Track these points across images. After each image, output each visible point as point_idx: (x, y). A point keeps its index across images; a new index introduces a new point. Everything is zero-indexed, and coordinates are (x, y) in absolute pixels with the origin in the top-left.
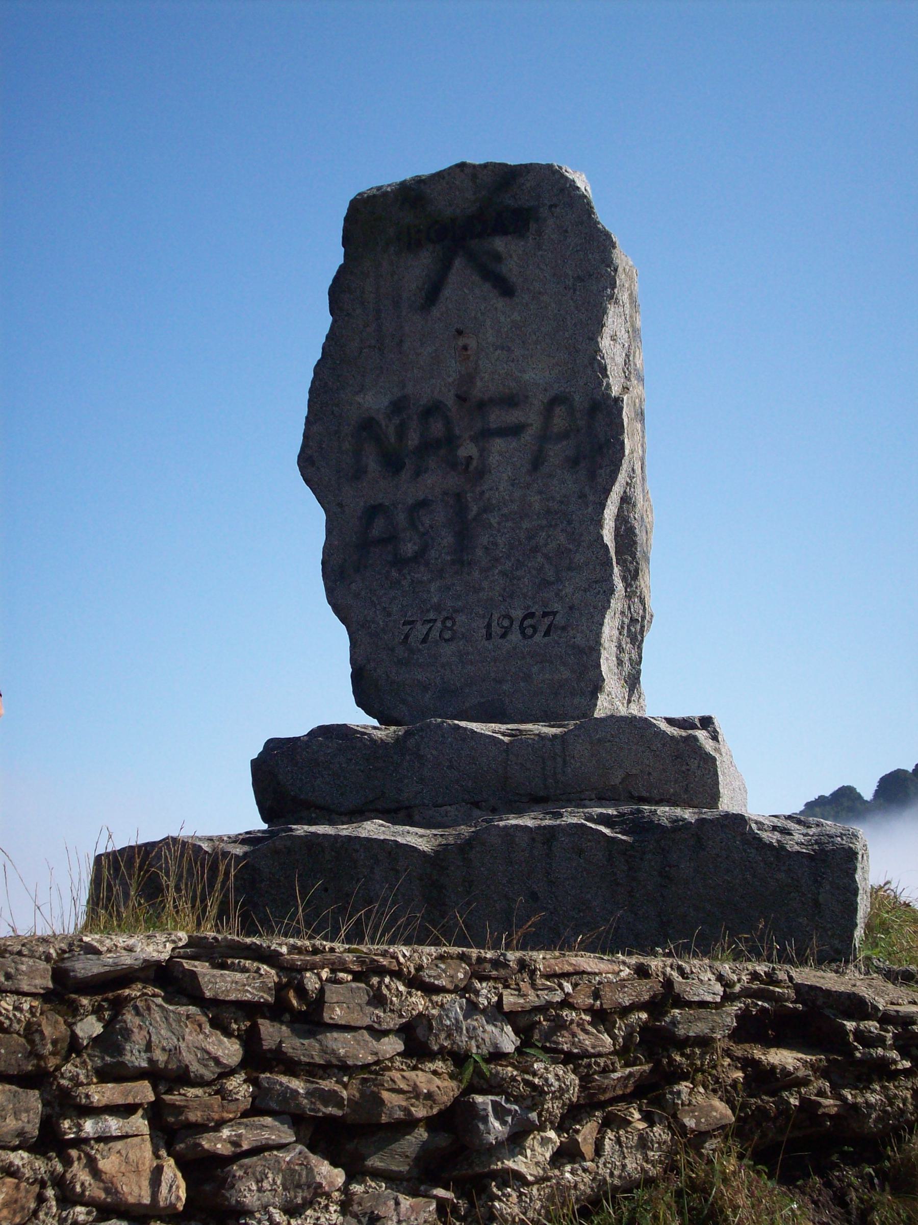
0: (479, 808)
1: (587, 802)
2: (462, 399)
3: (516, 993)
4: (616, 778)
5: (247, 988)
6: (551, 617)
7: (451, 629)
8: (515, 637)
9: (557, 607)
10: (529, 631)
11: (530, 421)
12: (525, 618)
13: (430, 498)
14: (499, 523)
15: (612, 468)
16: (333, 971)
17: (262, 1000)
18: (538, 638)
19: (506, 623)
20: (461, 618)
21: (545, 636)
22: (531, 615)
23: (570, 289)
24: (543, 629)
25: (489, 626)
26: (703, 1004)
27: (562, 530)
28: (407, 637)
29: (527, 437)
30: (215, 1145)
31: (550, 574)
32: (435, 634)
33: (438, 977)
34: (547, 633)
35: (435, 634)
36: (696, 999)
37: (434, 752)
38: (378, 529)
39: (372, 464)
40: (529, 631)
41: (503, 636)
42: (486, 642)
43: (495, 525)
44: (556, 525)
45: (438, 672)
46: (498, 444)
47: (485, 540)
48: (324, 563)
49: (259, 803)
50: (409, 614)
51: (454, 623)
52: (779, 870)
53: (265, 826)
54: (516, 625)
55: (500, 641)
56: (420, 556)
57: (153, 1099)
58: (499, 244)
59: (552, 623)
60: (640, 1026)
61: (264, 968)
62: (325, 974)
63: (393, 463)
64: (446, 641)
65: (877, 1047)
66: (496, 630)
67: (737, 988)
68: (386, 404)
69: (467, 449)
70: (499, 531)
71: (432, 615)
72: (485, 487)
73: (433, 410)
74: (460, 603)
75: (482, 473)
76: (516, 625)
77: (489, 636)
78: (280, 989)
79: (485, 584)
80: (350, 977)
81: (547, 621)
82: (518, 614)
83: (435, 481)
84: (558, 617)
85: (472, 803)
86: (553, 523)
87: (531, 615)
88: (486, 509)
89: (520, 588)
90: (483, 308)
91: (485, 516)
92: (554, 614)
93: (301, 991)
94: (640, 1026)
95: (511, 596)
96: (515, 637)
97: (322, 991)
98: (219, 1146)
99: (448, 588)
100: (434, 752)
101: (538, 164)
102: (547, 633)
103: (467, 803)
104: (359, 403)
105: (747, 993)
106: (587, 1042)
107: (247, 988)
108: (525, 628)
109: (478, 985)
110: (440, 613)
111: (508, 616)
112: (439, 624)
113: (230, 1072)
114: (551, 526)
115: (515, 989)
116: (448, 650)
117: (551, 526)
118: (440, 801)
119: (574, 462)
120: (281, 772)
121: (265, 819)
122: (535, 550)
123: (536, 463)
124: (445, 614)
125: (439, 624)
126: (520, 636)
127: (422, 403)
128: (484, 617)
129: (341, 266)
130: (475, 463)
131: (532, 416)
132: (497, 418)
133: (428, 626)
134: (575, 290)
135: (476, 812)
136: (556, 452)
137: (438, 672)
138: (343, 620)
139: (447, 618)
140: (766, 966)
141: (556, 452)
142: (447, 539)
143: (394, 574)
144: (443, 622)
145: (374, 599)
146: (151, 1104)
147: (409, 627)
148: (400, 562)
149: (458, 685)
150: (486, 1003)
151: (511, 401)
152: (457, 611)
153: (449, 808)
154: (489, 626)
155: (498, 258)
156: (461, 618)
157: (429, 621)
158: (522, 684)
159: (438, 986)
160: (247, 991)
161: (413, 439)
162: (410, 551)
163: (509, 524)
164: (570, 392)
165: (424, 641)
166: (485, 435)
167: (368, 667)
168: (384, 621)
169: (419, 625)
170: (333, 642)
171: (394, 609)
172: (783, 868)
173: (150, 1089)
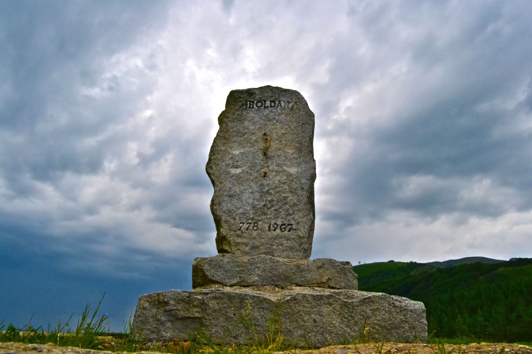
4: (324, 280)
7: (256, 226)
9: (293, 222)
10: (283, 230)
18: (286, 232)
20: (260, 223)
22: (284, 224)
24: (288, 229)
25: (269, 227)
31: (291, 211)
32: (251, 227)
34: (289, 231)
35: (251, 227)
40: (283, 230)
41: (274, 230)
64: (255, 230)
71: (250, 221)
76: (279, 227)
77: (269, 230)
79: (269, 212)
81: (289, 227)
82: (279, 223)
84: (293, 226)
87: (284, 224)
92: (292, 225)
99: (256, 213)
102: (289, 231)
111: (276, 224)
112: (252, 225)
116: (255, 233)
118: (264, 283)
122: (286, 203)
125: (252, 225)
128: (268, 224)
139: (255, 223)
152: (259, 221)
156: (260, 223)
157: (249, 223)
163: (278, 194)
165: (247, 229)
169: (245, 224)
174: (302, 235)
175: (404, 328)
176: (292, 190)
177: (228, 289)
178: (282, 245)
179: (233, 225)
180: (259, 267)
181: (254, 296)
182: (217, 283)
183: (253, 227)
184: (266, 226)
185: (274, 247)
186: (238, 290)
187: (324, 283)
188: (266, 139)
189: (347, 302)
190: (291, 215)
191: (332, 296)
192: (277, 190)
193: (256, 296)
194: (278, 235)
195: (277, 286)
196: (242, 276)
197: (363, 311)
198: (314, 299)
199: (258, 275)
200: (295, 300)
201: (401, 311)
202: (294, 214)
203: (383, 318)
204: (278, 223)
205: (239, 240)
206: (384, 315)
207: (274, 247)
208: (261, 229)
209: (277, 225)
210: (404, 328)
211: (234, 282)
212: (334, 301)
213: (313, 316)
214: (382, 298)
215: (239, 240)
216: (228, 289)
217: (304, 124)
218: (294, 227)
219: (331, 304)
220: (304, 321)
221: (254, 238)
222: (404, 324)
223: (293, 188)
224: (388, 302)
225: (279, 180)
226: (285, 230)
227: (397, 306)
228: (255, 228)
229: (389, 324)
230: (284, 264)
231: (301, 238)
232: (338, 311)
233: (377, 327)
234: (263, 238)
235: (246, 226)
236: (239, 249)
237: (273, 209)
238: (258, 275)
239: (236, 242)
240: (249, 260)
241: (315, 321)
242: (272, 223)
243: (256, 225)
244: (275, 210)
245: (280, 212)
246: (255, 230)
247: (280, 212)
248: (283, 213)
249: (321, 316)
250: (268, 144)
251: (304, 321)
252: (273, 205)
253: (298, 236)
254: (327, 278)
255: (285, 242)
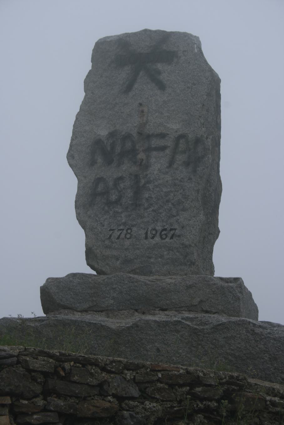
0: (137, 312)
1: (184, 312)
2: (140, 134)
3: (141, 375)
4: (196, 301)
5: (44, 366)
6: (174, 231)
7: (129, 233)
8: (157, 239)
9: (176, 226)
10: (164, 236)
11: (169, 145)
12: (163, 230)
13: (124, 176)
14: (153, 189)
15: (204, 168)
16: (75, 363)
17: (50, 371)
18: (167, 240)
19: (154, 232)
20: (134, 229)
21: (170, 239)
22: (165, 230)
23: (190, 88)
24: (170, 235)
25: (146, 233)
26: (210, 385)
27: (181, 194)
28: (111, 236)
29: (168, 151)
30: (31, 420)
31: (174, 212)
32: (123, 236)
33: (112, 368)
34: (172, 238)
35: (123, 236)
36: (208, 383)
37: (119, 287)
38: (100, 188)
39: (100, 160)
40: (164, 236)
41: (153, 238)
42: (145, 241)
43: (152, 190)
44: (178, 191)
45: (124, 252)
46: (154, 153)
47: (147, 196)
48: (76, 202)
49: (42, 305)
50: (112, 226)
51: (131, 231)
52: (261, 344)
53: (45, 315)
54: (158, 234)
55: (151, 240)
56: (118, 202)
57: (11, 403)
58: (159, 66)
59: (174, 233)
60: (186, 392)
61: (51, 360)
62: (72, 363)
63: (109, 161)
64: (128, 239)
65: (278, 407)
66: (149, 235)
67: (224, 380)
68: (107, 133)
69: (141, 156)
70: (153, 192)
71: (122, 227)
72: (148, 172)
73: (128, 137)
74: (134, 223)
75: (147, 167)
76: (158, 234)
77: (146, 238)
78: (56, 367)
79: (146, 214)
80: (81, 366)
81: (172, 232)
82: (159, 228)
83: (127, 168)
84: (177, 231)
85: (134, 310)
86: (177, 190)
87: (165, 230)
88: (149, 182)
89: (161, 217)
90: (151, 94)
91: (147, 185)
92: (175, 229)
93: (64, 369)
94: (186, 392)
95: (157, 221)
96: (157, 239)
97: (71, 369)
98: (32, 421)
99: (130, 216)
100: (119, 287)
101: (179, 32)
102: (172, 238)
103: (132, 309)
104: (95, 132)
105: (228, 383)
106: (166, 396)
107: (44, 366)
108: (162, 235)
109: (126, 372)
110: (125, 226)
111: (154, 229)
112: (125, 231)
113: (36, 396)
114: (176, 191)
115: (140, 374)
116: (127, 243)
117: (176, 191)
119: (187, 164)
120: (52, 294)
121: (45, 312)
122: (168, 201)
123: (171, 163)
124: (127, 227)
125: (125, 231)
126: (160, 238)
127: (122, 134)
128: (144, 229)
129: (90, 71)
130: (144, 161)
131: (169, 142)
132: (155, 142)
133: (120, 232)
134: (192, 89)
135: (136, 314)
136: (180, 158)
137: (124, 252)
138: (84, 227)
139: (128, 229)
140: (237, 374)
141: (180, 158)
142: (130, 193)
143: (106, 208)
144: (127, 230)
145: (97, 218)
146: (10, 404)
147: (112, 232)
148: (109, 203)
149: (132, 258)
150: (129, 378)
151: (162, 136)
152: (133, 226)
153: (125, 311)
154: (146, 233)
155: (159, 73)
156: (134, 229)
157: (121, 230)
158: (159, 259)
159: (112, 371)
160: (45, 368)
161: (118, 149)
162: (114, 198)
163: (158, 189)
164: (187, 134)
165: (118, 238)
166: (149, 150)
167: (93, 248)
168: (101, 229)
169: (116, 231)
170: (77, 238)
171: (106, 223)
172: (262, 343)
173: (10, 399)
174: (187, 243)
175: (263, 359)
176: (176, 181)
177: (77, 316)
178: (162, 257)
179: (100, 232)
180: (114, 288)
181: (90, 323)
182: (65, 307)
183: (126, 235)
184: (142, 232)
185: (152, 260)
186: (88, 317)
187: (195, 306)
188: (143, 111)
189: (196, 329)
190: (174, 216)
191: (180, 321)
192: (156, 183)
193: (92, 323)
194: (157, 244)
195: (136, 310)
196: (94, 299)
197: (215, 340)
198: (159, 326)
199: (114, 298)
200: (137, 326)
201: (261, 339)
202: (178, 215)
203: (237, 347)
204: (157, 228)
205: (108, 252)
206: (239, 343)
207: (152, 260)
208: (135, 236)
209: (157, 231)
210: (263, 359)
211: (86, 306)
212: (182, 328)
213: (156, 344)
214: (239, 324)
215: (108, 252)
216: (77, 316)
217: (195, 85)
218: (178, 232)
219: (178, 331)
220: (147, 351)
221: (126, 249)
222: (264, 354)
223: (177, 179)
224: (246, 328)
225: (159, 169)
226: (166, 237)
227: (257, 334)
228: (128, 236)
229: (245, 354)
230: (146, 284)
231: (186, 246)
232: (186, 339)
233: (230, 357)
234: (138, 249)
235: (117, 233)
236: (107, 264)
237: (151, 209)
238: (114, 298)
239: (104, 256)
240: (104, 280)
241: (158, 350)
242: (150, 229)
243: (129, 231)
244: (153, 211)
245: (161, 213)
246: (128, 239)
247: (161, 213)
248: (164, 214)
249: (165, 344)
250: (145, 118)
251: (147, 351)
252: (151, 205)
253: (183, 244)
254: (199, 300)
255: (166, 253)
